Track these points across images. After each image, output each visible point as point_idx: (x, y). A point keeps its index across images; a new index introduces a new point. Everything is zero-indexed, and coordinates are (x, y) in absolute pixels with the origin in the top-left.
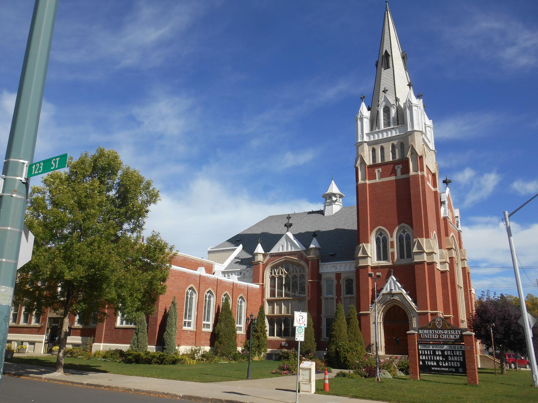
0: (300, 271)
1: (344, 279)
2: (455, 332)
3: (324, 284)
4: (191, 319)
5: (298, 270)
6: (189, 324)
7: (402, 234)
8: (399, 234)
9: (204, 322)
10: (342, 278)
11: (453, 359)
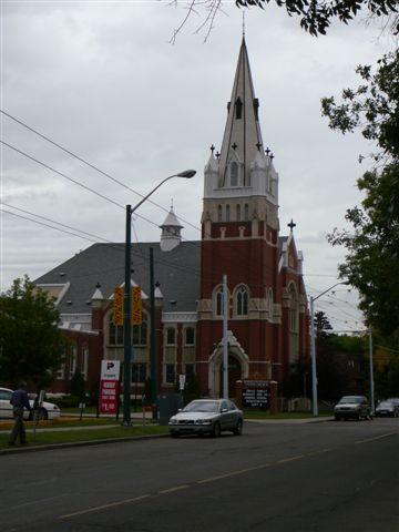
3: (165, 333)
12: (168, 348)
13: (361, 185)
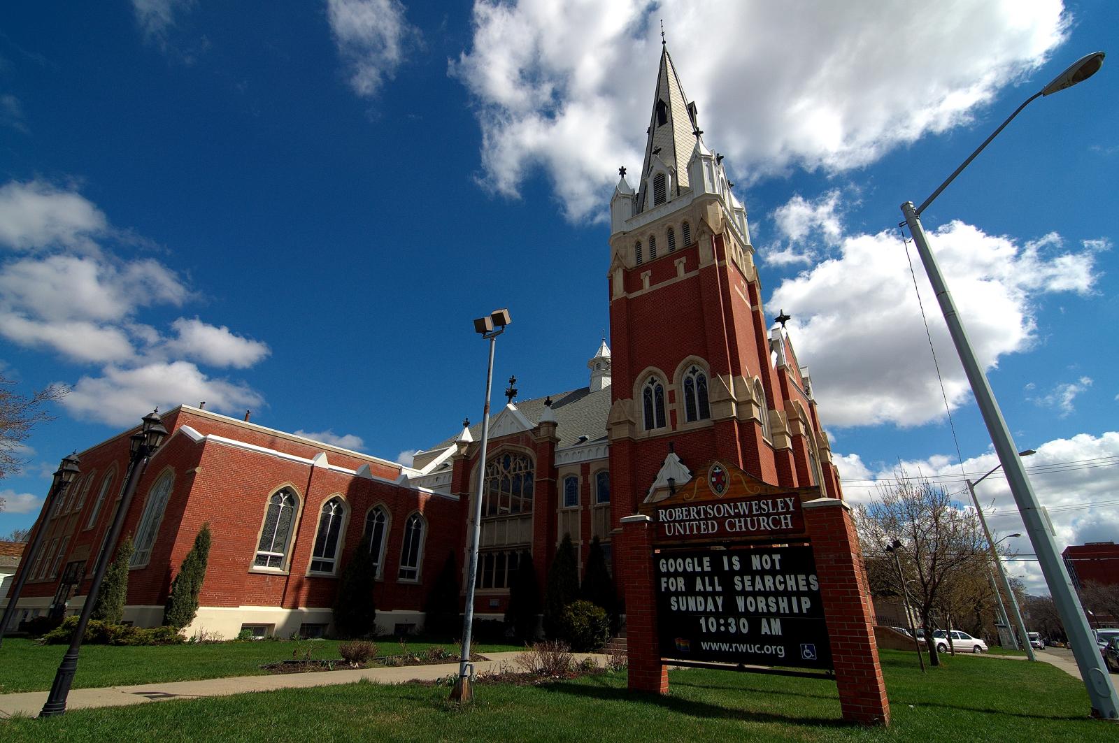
0: (526, 467)
1: (595, 473)
2: (775, 505)
3: (562, 487)
4: (414, 565)
5: (522, 465)
6: (412, 574)
7: (691, 375)
8: (685, 377)
9: (403, 567)
10: (591, 472)
11: (759, 586)
12: (564, 512)
13: (506, 395)
